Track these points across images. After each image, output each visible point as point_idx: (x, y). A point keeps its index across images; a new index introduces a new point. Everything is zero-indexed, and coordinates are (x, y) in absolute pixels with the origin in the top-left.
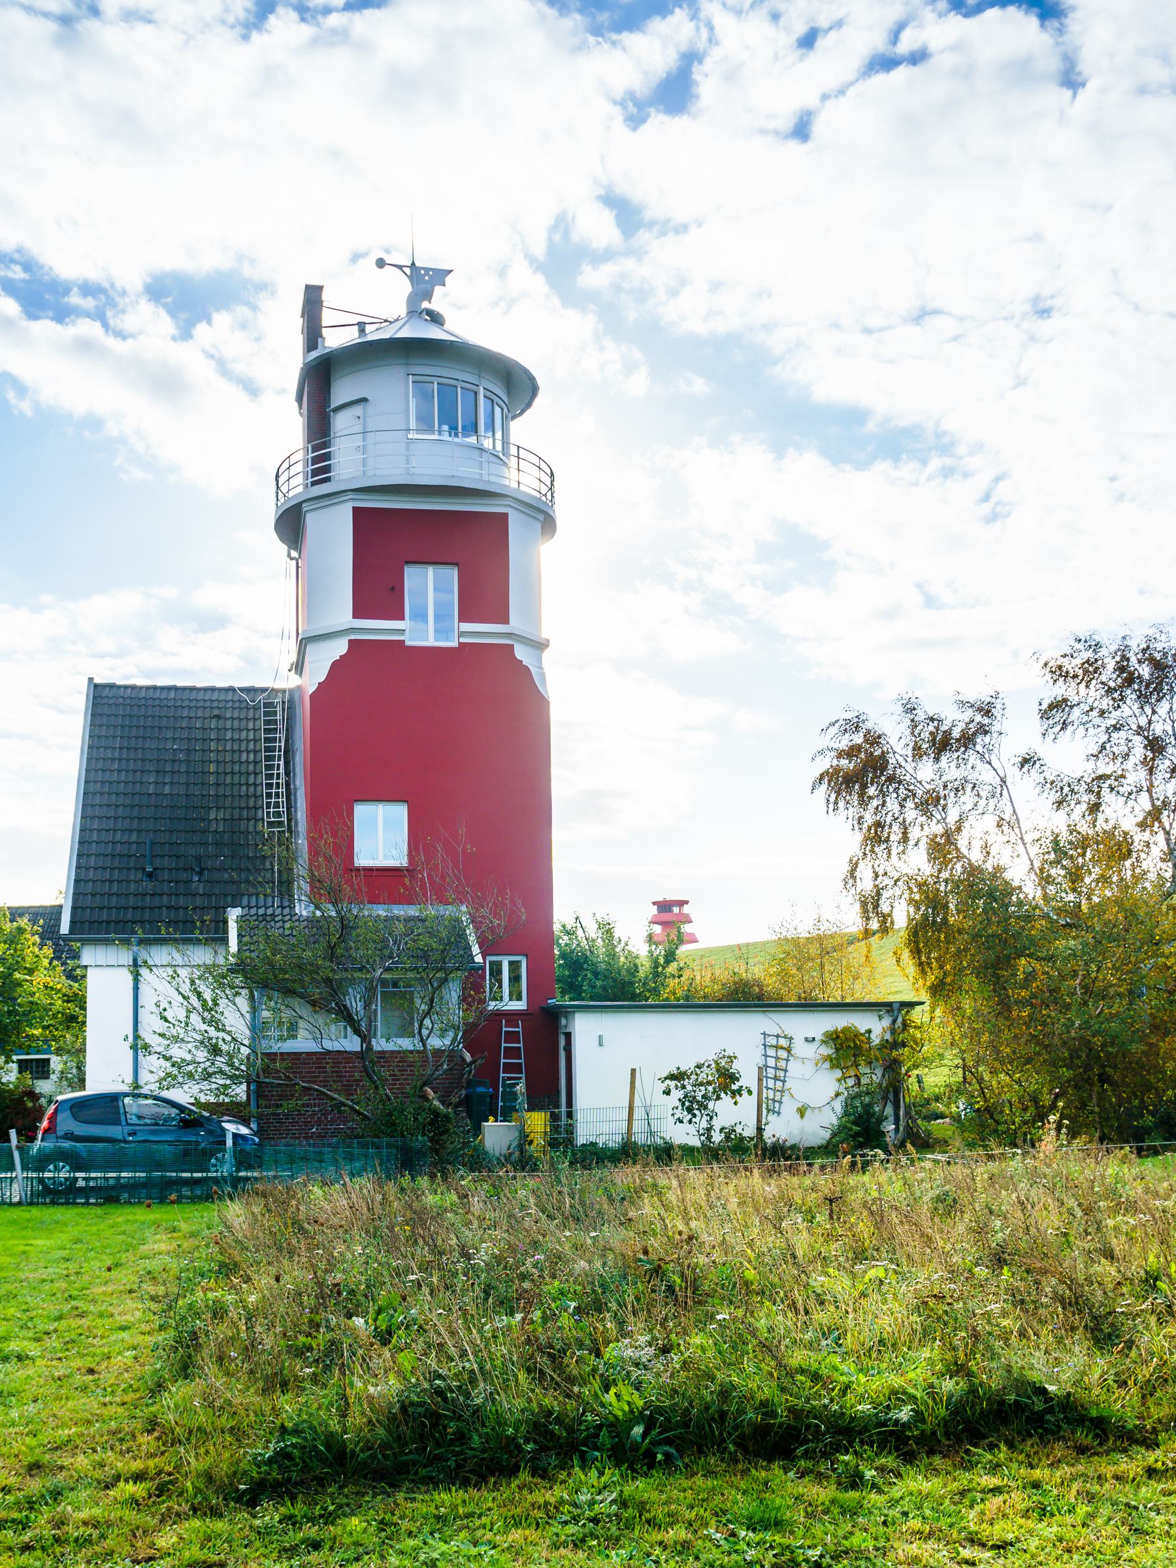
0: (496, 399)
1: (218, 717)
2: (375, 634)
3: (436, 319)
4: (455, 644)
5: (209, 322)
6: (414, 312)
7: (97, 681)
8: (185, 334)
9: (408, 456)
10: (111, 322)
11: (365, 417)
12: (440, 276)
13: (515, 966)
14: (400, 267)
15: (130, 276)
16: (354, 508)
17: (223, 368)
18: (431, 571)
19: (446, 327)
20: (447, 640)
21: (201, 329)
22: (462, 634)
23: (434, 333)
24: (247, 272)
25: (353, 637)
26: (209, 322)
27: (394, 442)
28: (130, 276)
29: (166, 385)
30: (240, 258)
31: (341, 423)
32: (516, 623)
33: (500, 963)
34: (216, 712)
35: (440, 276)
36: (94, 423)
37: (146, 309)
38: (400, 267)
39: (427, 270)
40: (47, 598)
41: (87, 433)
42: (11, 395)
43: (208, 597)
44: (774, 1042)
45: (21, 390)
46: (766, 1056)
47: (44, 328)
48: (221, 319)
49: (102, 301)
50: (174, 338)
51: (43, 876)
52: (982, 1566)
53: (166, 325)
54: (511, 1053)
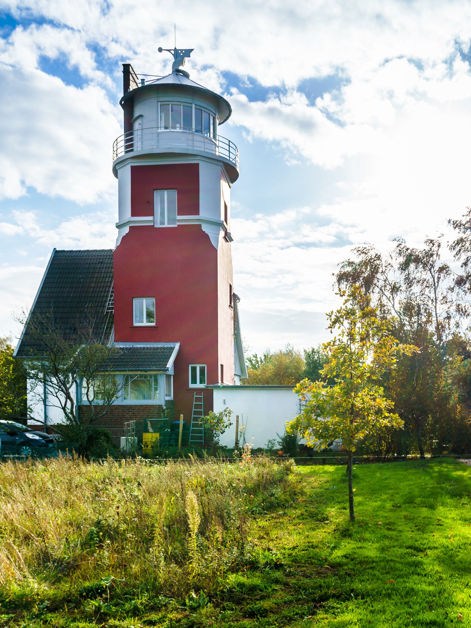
0: (203, 109)
1: (102, 263)
2: (140, 223)
3: (186, 75)
4: (176, 226)
5: (322, 98)
6: (177, 71)
7: (57, 249)
8: (312, 103)
9: (158, 140)
10: (282, 99)
11: (142, 124)
12: (188, 53)
13: (202, 370)
14: (169, 51)
15: (292, 82)
16: (131, 166)
17: (329, 116)
18: (166, 193)
19: (190, 78)
20: (173, 224)
21: (319, 101)
22: (179, 221)
23: (185, 82)
24: (340, 75)
25: (131, 225)
26: (322, 98)
27: (163, 135)
28: (292, 82)
29: (306, 126)
30: (337, 69)
31: (137, 126)
32: (204, 213)
33: (196, 367)
34: (101, 261)
35: (188, 53)
36: (277, 143)
37: (296, 95)
38: (169, 51)
39: (182, 50)
40: (259, 216)
41: (273, 147)
42: (244, 134)
43: (324, 210)
44: (304, 403)
45: (248, 131)
46: (300, 410)
47: (257, 106)
48: (327, 96)
49: (279, 91)
50: (307, 105)
51: (12, 333)
52: (470, 618)
53: (304, 99)
54: (197, 406)
